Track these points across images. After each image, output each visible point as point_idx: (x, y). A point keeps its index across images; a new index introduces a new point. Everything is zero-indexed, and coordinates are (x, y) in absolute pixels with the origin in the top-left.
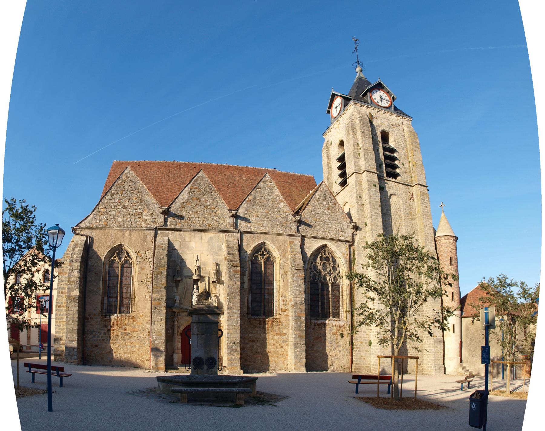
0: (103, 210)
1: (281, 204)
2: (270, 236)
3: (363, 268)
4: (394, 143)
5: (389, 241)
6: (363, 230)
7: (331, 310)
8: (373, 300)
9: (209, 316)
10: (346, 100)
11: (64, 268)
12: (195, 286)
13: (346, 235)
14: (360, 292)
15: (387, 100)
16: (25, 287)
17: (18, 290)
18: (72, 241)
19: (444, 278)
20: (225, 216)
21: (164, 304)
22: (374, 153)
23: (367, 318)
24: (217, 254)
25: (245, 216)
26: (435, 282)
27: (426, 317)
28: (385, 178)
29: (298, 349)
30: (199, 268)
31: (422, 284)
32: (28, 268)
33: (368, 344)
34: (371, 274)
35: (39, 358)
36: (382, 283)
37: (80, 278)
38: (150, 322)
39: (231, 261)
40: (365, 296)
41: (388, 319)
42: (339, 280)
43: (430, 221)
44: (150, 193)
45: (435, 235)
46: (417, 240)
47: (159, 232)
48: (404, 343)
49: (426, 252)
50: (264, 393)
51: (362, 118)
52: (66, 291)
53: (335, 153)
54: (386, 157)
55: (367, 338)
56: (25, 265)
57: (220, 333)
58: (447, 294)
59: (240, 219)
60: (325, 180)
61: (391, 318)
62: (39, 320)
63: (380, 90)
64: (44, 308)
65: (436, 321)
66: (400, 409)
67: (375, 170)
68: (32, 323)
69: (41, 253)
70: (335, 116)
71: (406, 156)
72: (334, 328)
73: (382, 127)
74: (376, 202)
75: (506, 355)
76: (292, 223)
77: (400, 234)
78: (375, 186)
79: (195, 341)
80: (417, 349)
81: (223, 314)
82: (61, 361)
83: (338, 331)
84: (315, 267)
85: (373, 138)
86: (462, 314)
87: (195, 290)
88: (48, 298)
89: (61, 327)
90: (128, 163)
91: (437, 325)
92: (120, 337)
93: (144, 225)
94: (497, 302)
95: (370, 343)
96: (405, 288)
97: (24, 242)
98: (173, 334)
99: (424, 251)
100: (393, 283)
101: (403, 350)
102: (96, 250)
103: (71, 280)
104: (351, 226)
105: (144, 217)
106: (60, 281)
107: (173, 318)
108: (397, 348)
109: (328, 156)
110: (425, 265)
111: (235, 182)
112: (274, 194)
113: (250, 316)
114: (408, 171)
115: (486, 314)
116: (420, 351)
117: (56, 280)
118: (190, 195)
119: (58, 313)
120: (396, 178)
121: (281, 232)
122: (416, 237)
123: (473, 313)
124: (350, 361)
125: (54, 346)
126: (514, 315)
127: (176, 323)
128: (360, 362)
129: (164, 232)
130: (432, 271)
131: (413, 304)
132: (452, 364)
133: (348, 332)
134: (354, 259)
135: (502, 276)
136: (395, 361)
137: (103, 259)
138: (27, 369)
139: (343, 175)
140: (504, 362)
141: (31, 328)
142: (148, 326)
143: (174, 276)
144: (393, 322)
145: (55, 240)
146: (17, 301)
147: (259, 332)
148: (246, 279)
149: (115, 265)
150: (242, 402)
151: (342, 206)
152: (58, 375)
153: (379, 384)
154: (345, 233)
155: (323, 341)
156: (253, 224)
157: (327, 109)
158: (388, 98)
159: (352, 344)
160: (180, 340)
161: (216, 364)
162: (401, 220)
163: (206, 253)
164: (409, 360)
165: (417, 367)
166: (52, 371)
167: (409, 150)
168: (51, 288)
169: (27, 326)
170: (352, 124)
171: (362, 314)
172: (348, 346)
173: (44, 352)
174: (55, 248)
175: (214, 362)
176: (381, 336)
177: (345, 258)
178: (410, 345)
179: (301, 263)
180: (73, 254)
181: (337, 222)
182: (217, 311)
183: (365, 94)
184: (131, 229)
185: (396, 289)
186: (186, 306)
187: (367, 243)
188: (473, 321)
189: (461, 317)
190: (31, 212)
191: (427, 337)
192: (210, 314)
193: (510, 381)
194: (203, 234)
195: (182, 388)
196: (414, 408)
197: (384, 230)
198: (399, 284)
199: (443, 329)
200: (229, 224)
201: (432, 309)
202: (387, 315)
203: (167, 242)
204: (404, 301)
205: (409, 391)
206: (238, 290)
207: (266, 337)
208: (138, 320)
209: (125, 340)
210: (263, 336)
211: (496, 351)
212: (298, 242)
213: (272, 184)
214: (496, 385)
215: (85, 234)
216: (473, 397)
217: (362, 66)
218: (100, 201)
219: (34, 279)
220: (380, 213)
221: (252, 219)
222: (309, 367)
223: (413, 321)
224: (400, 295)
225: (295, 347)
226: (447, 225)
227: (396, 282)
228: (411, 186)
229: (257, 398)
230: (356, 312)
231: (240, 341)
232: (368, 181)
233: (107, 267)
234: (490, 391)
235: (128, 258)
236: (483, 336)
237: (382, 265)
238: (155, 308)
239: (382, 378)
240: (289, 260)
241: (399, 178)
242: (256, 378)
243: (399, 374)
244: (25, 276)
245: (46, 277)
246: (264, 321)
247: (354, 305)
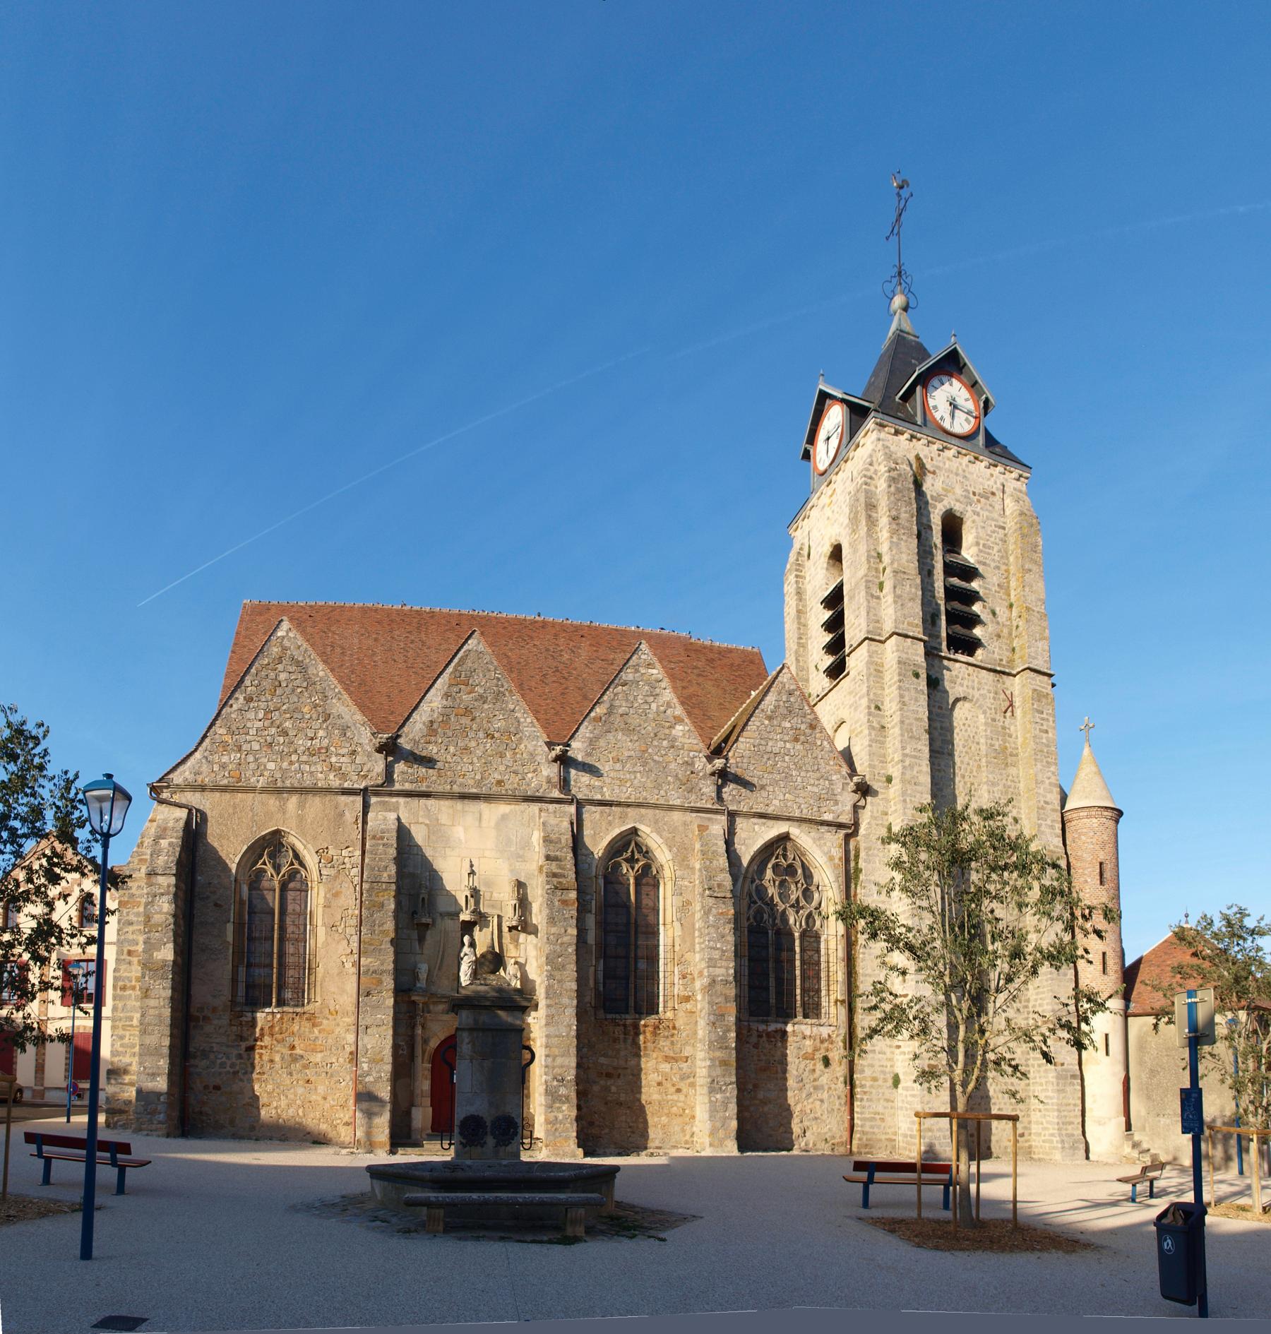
0: (228, 738)
1: (679, 727)
2: (650, 812)
3: (879, 893)
4: (974, 550)
5: (947, 822)
6: (880, 796)
7: (798, 998)
8: (904, 973)
9: (501, 1013)
10: (857, 414)
11: (134, 891)
12: (466, 939)
13: (839, 808)
14: (870, 954)
15: (969, 413)
16: (30, 938)
17: (10, 945)
18: (152, 821)
19: (1083, 916)
20: (538, 758)
21: (389, 983)
22: (918, 581)
23: (887, 1018)
24: (520, 858)
25: (589, 760)
26: (1059, 926)
27: (1036, 1016)
29: (718, 1096)
30: (475, 893)
31: (1027, 933)
32: (38, 889)
33: (890, 1082)
34: (899, 907)
35: (65, 1119)
36: (925, 930)
37: (174, 916)
38: (353, 1028)
39: (555, 875)
40: (884, 963)
41: (940, 1021)
42: (818, 923)
43: (1052, 769)
44: (346, 696)
45: (1063, 806)
46: (1016, 820)
47: (373, 800)
48: (981, 1081)
49: (1038, 851)
50: (634, 1206)
51: (894, 474)
52: (140, 948)
53: (819, 582)
54: (951, 593)
55: (888, 1069)
56: (30, 880)
57: (527, 1055)
58: (1090, 957)
59: (576, 769)
60: (790, 660)
61: (948, 1018)
62: (69, 1023)
63: (952, 376)
64: (83, 990)
65: (1062, 1026)
66: (978, 1249)
67: (918, 632)
68: (51, 1030)
69: (70, 851)
70: (822, 467)
71: (1004, 587)
72: (808, 1042)
73: (945, 502)
74: (917, 719)
75: (1245, 1111)
76: (704, 777)
77: (973, 806)
78: (917, 675)
79: (465, 1075)
80: (1014, 1095)
81: (536, 1007)
82: (125, 1127)
83: (816, 1050)
84: (761, 891)
85: (919, 536)
86: (1127, 1007)
87: (466, 949)
88: (92, 966)
89: (126, 1041)
90: (283, 610)
91: (1064, 1034)
92: (278, 1066)
93: (335, 783)
94: (1220, 977)
95: (896, 1081)
96: (983, 942)
97: (23, 820)
98: (412, 1057)
99: (1033, 847)
100: (952, 930)
101: (979, 1098)
102: (215, 845)
103: (153, 922)
104: (852, 786)
105: (334, 759)
106: (124, 923)
107: (412, 1017)
108: (964, 1092)
109: (799, 593)
110: (1036, 885)
111: (561, 667)
113: (601, 1014)
114: (1005, 630)
115: (1192, 1008)
116: (1022, 1101)
117: (112, 920)
118: (449, 703)
119: (120, 1005)
120: (971, 654)
121: (678, 802)
122: (1014, 813)
123: (1157, 1005)
124: (847, 1125)
125: (107, 1088)
126: (1265, 1009)
127: (419, 1031)
128: (872, 1127)
129: (387, 799)
130: (1053, 900)
131: (1002, 982)
132: (1104, 1132)
133: (843, 1052)
134: (858, 871)
135: (1235, 909)
136: (959, 1126)
137: (234, 867)
138: (33, 1148)
139: (836, 646)
140: (1243, 1129)
141: (48, 1044)
142: (351, 1038)
143: (415, 913)
144: (953, 1027)
145: (106, 817)
146: (10, 973)
147: (622, 1053)
148: (591, 920)
149: (265, 884)
150: (580, 1231)
151: (830, 732)
152: (114, 1163)
153: (920, 1183)
154: (836, 803)
155: (780, 1075)
156: (608, 780)
157: (804, 445)
158: (970, 405)
159: (851, 1082)
160: (428, 1074)
161: (516, 1134)
162: (979, 767)
163: (491, 853)
164: (995, 1123)
165: (1016, 1141)
166: (99, 1154)
167: (1012, 569)
168: (100, 941)
169: (37, 1038)
170: (867, 492)
171: (875, 1008)
172: (841, 1089)
173: (79, 1103)
174: (106, 837)
175: (512, 1128)
176: (924, 1063)
177: (836, 867)
178: (996, 1085)
179: (727, 880)
180: (156, 853)
181: (818, 775)
182: (520, 1001)
183: (908, 396)
184: (302, 791)
185: (961, 945)
186: (444, 987)
187: (889, 829)
188: (1156, 1026)
189: (1126, 1016)
190: (37, 741)
191: (1039, 1066)
192: (502, 1008)
193: (1261, 1178)
194: (483, 806)
195: (432, 1195)
196: (1013, 1248)
197: (934, 796)
198: (967, 932)
199: (1079, 1046)
200: (549, 781)
201: (1051, 995)
202: (937, 1011)
203: (394, 826)
204: (981, 975)
205: (996, 1203)
206: (571, 949)
207: (639, 1065)
208: (325, 1022)
209: (291, 1074)
210: (633, 1062)
211: (1218, 1101)
212: (718, 826)
213: (657, 672)
214: (1224, 1189)
215: (184, 801)
216: (1164, 1221)
217: (908, 292)
218: (219, 714)
219: (55, 917)
220: (927, 750)
221: (605, 767)
222: (745, 1140)
223: (1003, 1025)
224: (970, 960)
225: (712, 1091)
226: (1097, 779)
227: (962, 927)
228: (1009, 674)
229: (618, 1218)
230: (860, 1004)
231: (577, 1076)
232: (899, 662)
233: (245, 889)
234: (1209, 1204)
235: (296, 866)
236: (1183, 1064)
237: (926, 885)
238: (368, 994)
239: (927, 1168)
240: (697, 873)
241: (979, 652)
242: (616, 1169)
243: (971, 1158)
244: (30, 908)
245: (86, 913)
246: (636, 1026)
247: (857, 987)
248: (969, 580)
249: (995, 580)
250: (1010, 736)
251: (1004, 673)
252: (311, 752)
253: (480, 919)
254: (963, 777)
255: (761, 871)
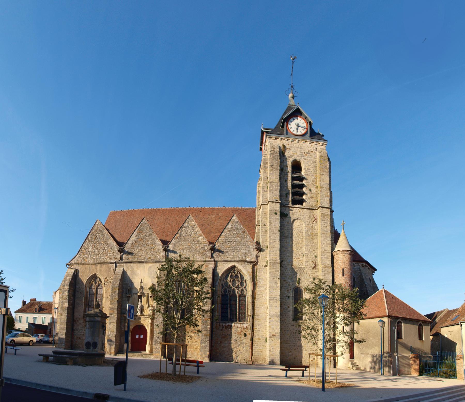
0: (84, 251)
1: (200, 237)
25: (174, 250)
28: (290, 205)
30: (142, 288)
33: (265, 340)
47: (118, 265)
51: (272, 152)
54: (294, 186)
63: (298, 116)
71: (315, 182)
72: (239, 329)
74: (276, 227)
76: (208, 251)
78: (276, 214)
83: (242, 331)
87: (139, 303)
93: (109, 261)
112: (195, 230)
114: (315, 196)
120: (302, 205)
121: (200, 259)
133: (250, 332)
137: (85, 283)
154: (251, 255)
155: (229, 339)
158: (305, 125)
163: (145, 276)
167: (318, 175)
181: (245, 247)
184: (101, 263)
194: (145, 264)
200: (163, 256)
203: (122, 271)
228: (315, 209)
241: (304, 203)
242: (65, 349)
248: (302, 181)
249: (312, 180)
250: (315, 229)
251: (313, 209)
252: (103, 253)
253: (143, 295)
254: (296, 244)
255: (227, 277)
